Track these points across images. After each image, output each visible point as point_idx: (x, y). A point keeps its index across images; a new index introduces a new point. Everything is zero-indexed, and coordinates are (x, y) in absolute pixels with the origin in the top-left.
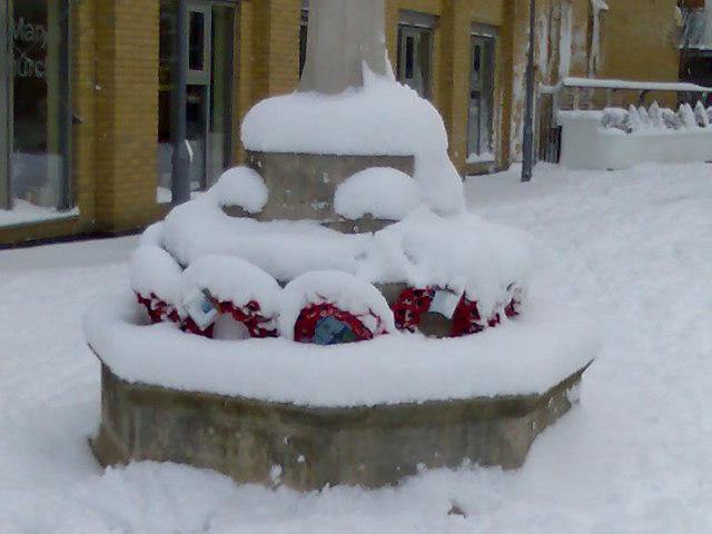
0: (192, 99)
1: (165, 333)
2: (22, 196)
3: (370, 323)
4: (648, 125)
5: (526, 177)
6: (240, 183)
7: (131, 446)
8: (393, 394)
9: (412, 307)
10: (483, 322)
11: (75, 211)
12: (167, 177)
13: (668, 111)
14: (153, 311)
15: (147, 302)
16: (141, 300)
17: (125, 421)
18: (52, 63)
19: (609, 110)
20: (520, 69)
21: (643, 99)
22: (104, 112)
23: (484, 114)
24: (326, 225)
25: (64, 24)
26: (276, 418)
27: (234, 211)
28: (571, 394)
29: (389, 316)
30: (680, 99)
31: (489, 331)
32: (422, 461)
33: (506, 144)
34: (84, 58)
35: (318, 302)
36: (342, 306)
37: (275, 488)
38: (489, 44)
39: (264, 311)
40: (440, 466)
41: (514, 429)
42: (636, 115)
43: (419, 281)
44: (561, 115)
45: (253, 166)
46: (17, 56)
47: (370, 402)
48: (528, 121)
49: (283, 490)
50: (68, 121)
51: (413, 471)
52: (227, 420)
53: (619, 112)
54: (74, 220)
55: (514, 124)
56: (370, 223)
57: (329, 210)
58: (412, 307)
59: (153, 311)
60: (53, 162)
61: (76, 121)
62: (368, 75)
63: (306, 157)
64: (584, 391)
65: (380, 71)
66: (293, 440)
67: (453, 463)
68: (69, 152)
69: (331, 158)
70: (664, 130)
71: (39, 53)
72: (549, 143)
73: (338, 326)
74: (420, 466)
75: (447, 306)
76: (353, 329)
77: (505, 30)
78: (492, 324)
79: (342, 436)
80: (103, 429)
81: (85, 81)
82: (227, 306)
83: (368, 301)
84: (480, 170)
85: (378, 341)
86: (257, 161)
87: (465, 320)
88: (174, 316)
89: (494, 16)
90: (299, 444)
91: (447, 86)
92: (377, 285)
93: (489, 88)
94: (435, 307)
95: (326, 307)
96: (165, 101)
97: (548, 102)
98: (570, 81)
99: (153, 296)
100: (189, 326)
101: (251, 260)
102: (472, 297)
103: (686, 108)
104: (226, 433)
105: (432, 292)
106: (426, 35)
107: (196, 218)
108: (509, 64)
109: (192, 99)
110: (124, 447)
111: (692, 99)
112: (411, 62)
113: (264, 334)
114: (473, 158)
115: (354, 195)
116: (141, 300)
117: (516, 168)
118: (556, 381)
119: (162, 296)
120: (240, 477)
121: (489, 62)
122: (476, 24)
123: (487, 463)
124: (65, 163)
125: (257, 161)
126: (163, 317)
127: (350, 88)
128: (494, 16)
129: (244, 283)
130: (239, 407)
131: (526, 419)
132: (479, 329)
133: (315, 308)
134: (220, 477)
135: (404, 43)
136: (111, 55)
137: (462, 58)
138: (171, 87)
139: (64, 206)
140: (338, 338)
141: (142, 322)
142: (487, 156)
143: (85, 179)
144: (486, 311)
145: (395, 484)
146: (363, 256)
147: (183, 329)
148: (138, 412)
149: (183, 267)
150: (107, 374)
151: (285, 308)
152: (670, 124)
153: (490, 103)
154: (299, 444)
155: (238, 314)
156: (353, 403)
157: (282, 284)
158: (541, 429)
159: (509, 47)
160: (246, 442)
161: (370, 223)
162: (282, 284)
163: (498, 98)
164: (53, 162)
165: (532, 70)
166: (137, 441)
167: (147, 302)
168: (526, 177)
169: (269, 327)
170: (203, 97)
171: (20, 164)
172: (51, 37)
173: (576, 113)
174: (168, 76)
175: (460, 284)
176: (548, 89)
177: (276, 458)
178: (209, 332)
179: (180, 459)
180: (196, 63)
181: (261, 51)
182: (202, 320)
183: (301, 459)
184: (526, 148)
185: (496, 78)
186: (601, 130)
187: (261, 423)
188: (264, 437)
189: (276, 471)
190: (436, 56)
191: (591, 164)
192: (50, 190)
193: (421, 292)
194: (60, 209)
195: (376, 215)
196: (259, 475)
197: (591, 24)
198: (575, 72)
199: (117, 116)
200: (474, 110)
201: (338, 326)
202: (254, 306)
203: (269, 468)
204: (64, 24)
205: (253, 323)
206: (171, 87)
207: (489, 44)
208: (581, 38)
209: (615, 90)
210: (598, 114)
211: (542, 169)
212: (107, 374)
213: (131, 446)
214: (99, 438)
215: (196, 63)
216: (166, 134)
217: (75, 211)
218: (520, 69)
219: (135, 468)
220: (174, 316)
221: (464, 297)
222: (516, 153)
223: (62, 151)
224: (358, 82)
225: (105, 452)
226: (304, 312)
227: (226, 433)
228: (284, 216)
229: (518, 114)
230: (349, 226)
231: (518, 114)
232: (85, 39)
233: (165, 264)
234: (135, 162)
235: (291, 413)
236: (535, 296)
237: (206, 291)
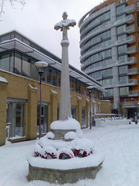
0: (42, 119)
1: (39, 158)
2: (17, 135)
3: (70, 156)
4: (108, 120)
5: (90, 129)
6: (50, 134)
7: (33, 178)
8: (74, 167)
9: (77, 153)
10: (87, 155)
11: (25, 137)
12: (38, 131)
13: (110, 118)
14: (37, 155)
15: (36, 153)
16: (35, 153)
17: (33, 174)
18: (22, 114)
19: (102, 118)
20: (89, 113)
21: (106, 116)
22: (29, 122)
23: (84, 120)
24: (63, 140)
25: (23, 109)
26: (57, 172)
27: (49, 138)
28: (101, 166)
29: (73, 154)
30: (112, 116)
31: (88, 156)
32: (80, 178)
33: (87, 123)
34: (26, 114)
35: (63, 153)
36: (66, 153)
37: (56, 184)
38: (84, 109)
39: (54, 154)
40: (82, 179)
41: (93, 172)
42: (106, 119)
43: (78, 149)
44: (95, 119)
45: (52, 132)
46: (17, 114)
47: (71, 169)
48: (90, 120)
49: (58, 184)
50: (24, 123)
51: (78, 180)
52: (48, 172)
53: (103, 118)
54: (24, 138)
55: (88, 121)
56: (70, 140)
57: (64, 138)
58: (77, 153)
59: (37, 155)
60: (21, 128)
61: (25, 123)
62: (69, 117)
63: (60, 130)
64: (103, 165)
65: (70, 117)
66: (59, 176)
67: (84, 179)
68: (24, 127)
69: (64, 130)
70: (110, 121)
71: (20, 113)
72: (93, 124)
73: (66, 156)
74: (79, 179)
75: (82, 152)
76: (68, 157)
77: (86, 107)
78: (89, 155)
79: (67, 174)
80: (29, 174)
81: (26, 117)
82: (49, 154)
83: (70, 152)
84: (84, 128)
85: (72, 158)
86: (52, 131)
87: (85, 155)
88: (41, 155)
89: (85, 106)
90: (60, 176)
91: (79, 116)
92: (71, 150)
93: (84, 115)
94: (80, 152)
95: (64, 153)
96: (38, 120)
97: (93, 117)
98: (96, 114)
99: (37, 152)
100: (43, 157)
101: (52, 146)
102: (85, 151)
103: (113, 117)
104: (48, 175)
105: (80, 150)
106: (75, 109)
107: (44, 140)
108: (87, 112)
109: (42, 119)
110: (32, 178)
111: (114, 116)
112: (74, 113)
113: (55, 158)
114: (83, 126)
115: (67, 136)
116: (35, 153)
117: (89, 127)
118: (99, 164)
119: (39, 152)
120: (51, 182)
121: (84, 112)
122: (82, 107)
123: (89, 178)
124: (23, 129)
125: (52, 131)
126: (39, 155)
127: (66, 120)
128: (85, 106)
129: (51, 150)
130: (51, 170)
131: (95, 170)
132: (87, 156)
133: (62, 154)
134: (48, 182)
135: (72, 110)
136: (30, 113)
137: (81, 112)
138: (39, 118)
139: (23, 136)
140: (66, 158)
141: (36, 156)
142: (85, 126)
143: (26, 132)
144: (88, 153)
145: (75, 183)
146: (69, 145)
147: (42, 157)
148: (35, 171)
149: (42, 147)
150: (30, 165)
151: (57, 154)
152: (111, 120)
153: (85, 118)
154: (60, 176)
155: (50, 155)
156: (68, 169)
157: (57, 150)
158: (97, 172)
159: (87, 110)
160: (52, 176)
161: (70, 140)
162: (57, 150)
163: (86, 117)
164: (21, 128)
165: (90, 113)
166: (34, 176)
167: (36, 153)
168: (90, 129)
169: (55, 157)
170: (43, 119)
171: (17, 129)
172: (22, 111)
173: (97, 119)
174: (38, 116)
175: (84, 149)
176: (93, 116)
177: (57, 179)
178: (46, 158)
179: (41, 180)
180: (42, 114)
181: (52, 115)
182: (45, 156)
183: (61, 179)
184: (90, 125)
185: (85, 115)
186: (101, 121)
187: (54, 173)
188: (55, 175)
189: (57, 181)
190: (77, 112)
191: (100, 126)
192: (21, 134)
193: (78, 150)
194: (22, 136)
195: (71, 139)
196: (54, 182)
197: (98, 106)
198: (97, 113)
199: (31, 122)
200: (82, 119)
201: (66, 156)
202: (53, 154)
203: (55, 181)
204: (23, 109)
205: (53, 156)
206: (39, 118)
207: (84, 109)
208: (97, 108)
209: (103, 115)
210: (100, 119)
211: (93, 127)
212: (30, 165)
213: (33, 178)
214: (28, 176)
215: (42, 114)
216: (38, 124)
217: (25, 137)
218: (89, 113)
219: (34, 181)
220: (41, 155)
221: (84, 151)
222: (89, 125)
223: (23, 127)
224: (67, 119)
225: (29, 178)
226: (60, 154)
227: (48, 175)
228: (57, 139)
229: (89, 119)
230: (67, 140)
231: (89, 119)
232: (27, 111)
233: (39, 147)
234: (34, 129)
235: (59, 171)
236: (95, 149)
237: (45, 151)
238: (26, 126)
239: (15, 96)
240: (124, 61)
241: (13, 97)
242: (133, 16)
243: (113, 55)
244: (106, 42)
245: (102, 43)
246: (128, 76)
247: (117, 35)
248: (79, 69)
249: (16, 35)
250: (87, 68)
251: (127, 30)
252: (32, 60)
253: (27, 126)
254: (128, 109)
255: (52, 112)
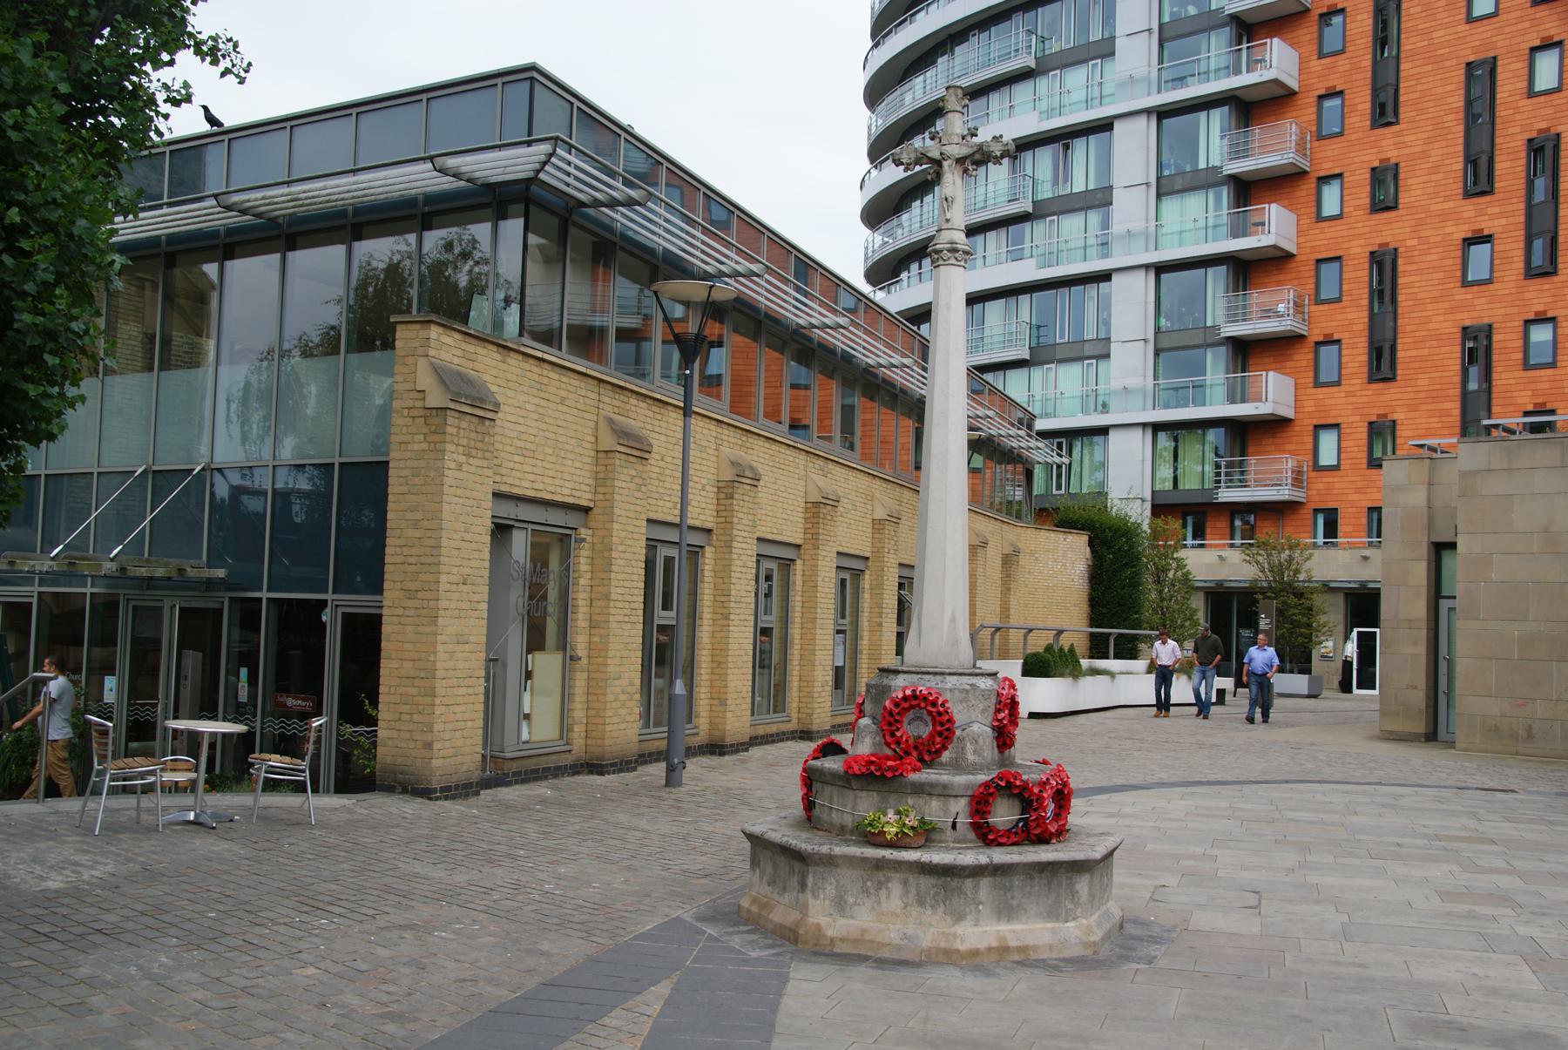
109: (663, 638)
215: (666, 606)
238: (578, 675)
239: (528, 484)
240: (1198, 393)
241: (515, 491)
242: (1283, 44)
243: (1118, 180)
244: (1076, 78)
245: (1042, 83)
246: (1223, 349)
247: (1161, 26)
248: (854, 273)
249: (537, 87)
250: (914, 267)
251: (1237, 153)
252: (622, 249)
253: (585, 675)
254: (1346, 594)
255: (723, 595)
